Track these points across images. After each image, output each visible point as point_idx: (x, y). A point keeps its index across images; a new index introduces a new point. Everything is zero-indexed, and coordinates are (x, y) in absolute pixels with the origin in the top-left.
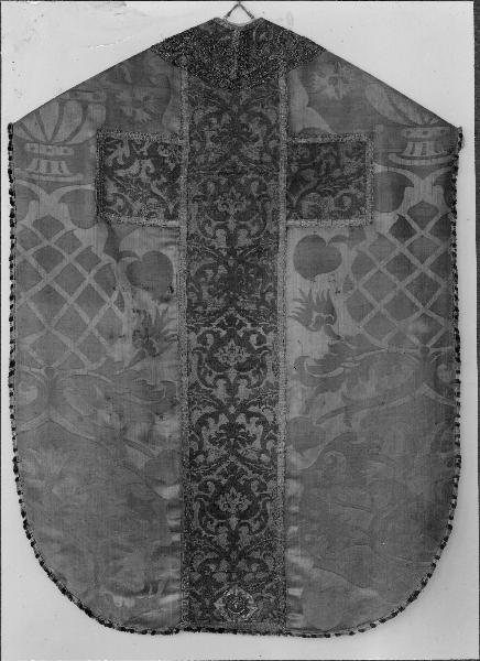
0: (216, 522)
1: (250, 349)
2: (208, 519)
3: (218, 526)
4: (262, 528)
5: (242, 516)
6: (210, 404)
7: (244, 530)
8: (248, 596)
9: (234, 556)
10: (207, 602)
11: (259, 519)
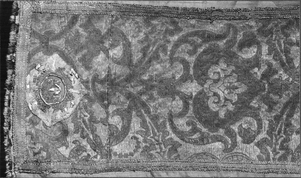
0: (192, 60)
1: (233, 117)
2: (196, 47)
3: (184, 62)
4: (181, 134)
5: (200, 101)
6: (144, 51)
7: (177, 104)
8: (69, 110)
9: (135, 89)
10: (60, 43)
11: (195, 130)
